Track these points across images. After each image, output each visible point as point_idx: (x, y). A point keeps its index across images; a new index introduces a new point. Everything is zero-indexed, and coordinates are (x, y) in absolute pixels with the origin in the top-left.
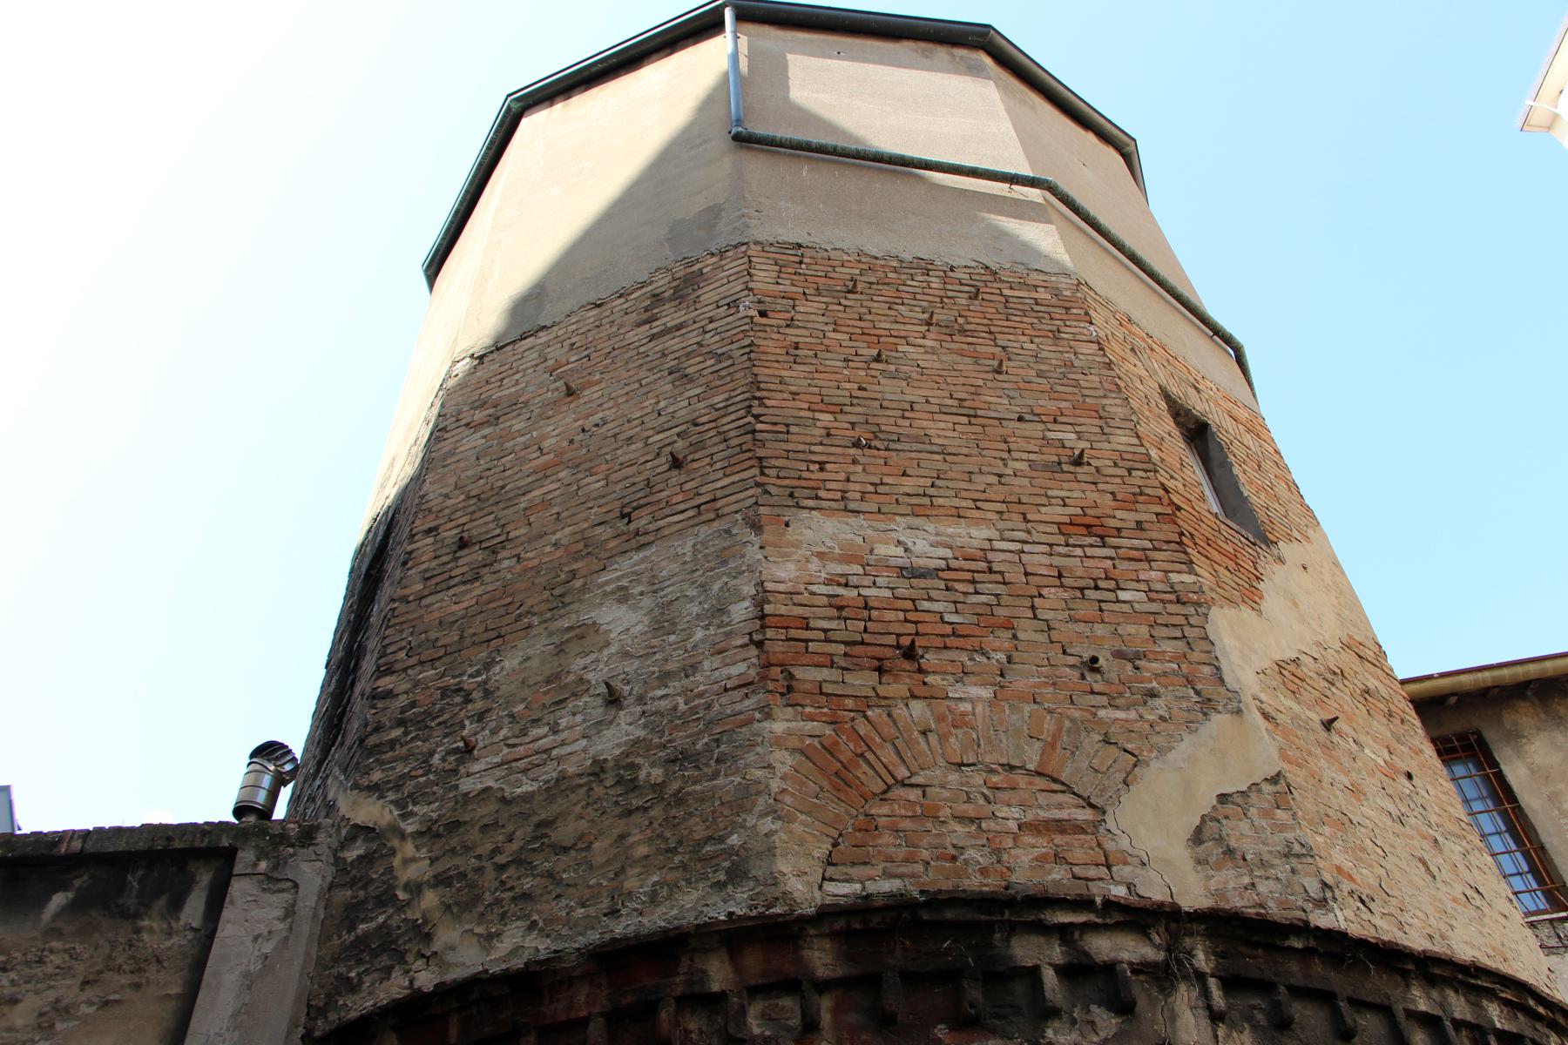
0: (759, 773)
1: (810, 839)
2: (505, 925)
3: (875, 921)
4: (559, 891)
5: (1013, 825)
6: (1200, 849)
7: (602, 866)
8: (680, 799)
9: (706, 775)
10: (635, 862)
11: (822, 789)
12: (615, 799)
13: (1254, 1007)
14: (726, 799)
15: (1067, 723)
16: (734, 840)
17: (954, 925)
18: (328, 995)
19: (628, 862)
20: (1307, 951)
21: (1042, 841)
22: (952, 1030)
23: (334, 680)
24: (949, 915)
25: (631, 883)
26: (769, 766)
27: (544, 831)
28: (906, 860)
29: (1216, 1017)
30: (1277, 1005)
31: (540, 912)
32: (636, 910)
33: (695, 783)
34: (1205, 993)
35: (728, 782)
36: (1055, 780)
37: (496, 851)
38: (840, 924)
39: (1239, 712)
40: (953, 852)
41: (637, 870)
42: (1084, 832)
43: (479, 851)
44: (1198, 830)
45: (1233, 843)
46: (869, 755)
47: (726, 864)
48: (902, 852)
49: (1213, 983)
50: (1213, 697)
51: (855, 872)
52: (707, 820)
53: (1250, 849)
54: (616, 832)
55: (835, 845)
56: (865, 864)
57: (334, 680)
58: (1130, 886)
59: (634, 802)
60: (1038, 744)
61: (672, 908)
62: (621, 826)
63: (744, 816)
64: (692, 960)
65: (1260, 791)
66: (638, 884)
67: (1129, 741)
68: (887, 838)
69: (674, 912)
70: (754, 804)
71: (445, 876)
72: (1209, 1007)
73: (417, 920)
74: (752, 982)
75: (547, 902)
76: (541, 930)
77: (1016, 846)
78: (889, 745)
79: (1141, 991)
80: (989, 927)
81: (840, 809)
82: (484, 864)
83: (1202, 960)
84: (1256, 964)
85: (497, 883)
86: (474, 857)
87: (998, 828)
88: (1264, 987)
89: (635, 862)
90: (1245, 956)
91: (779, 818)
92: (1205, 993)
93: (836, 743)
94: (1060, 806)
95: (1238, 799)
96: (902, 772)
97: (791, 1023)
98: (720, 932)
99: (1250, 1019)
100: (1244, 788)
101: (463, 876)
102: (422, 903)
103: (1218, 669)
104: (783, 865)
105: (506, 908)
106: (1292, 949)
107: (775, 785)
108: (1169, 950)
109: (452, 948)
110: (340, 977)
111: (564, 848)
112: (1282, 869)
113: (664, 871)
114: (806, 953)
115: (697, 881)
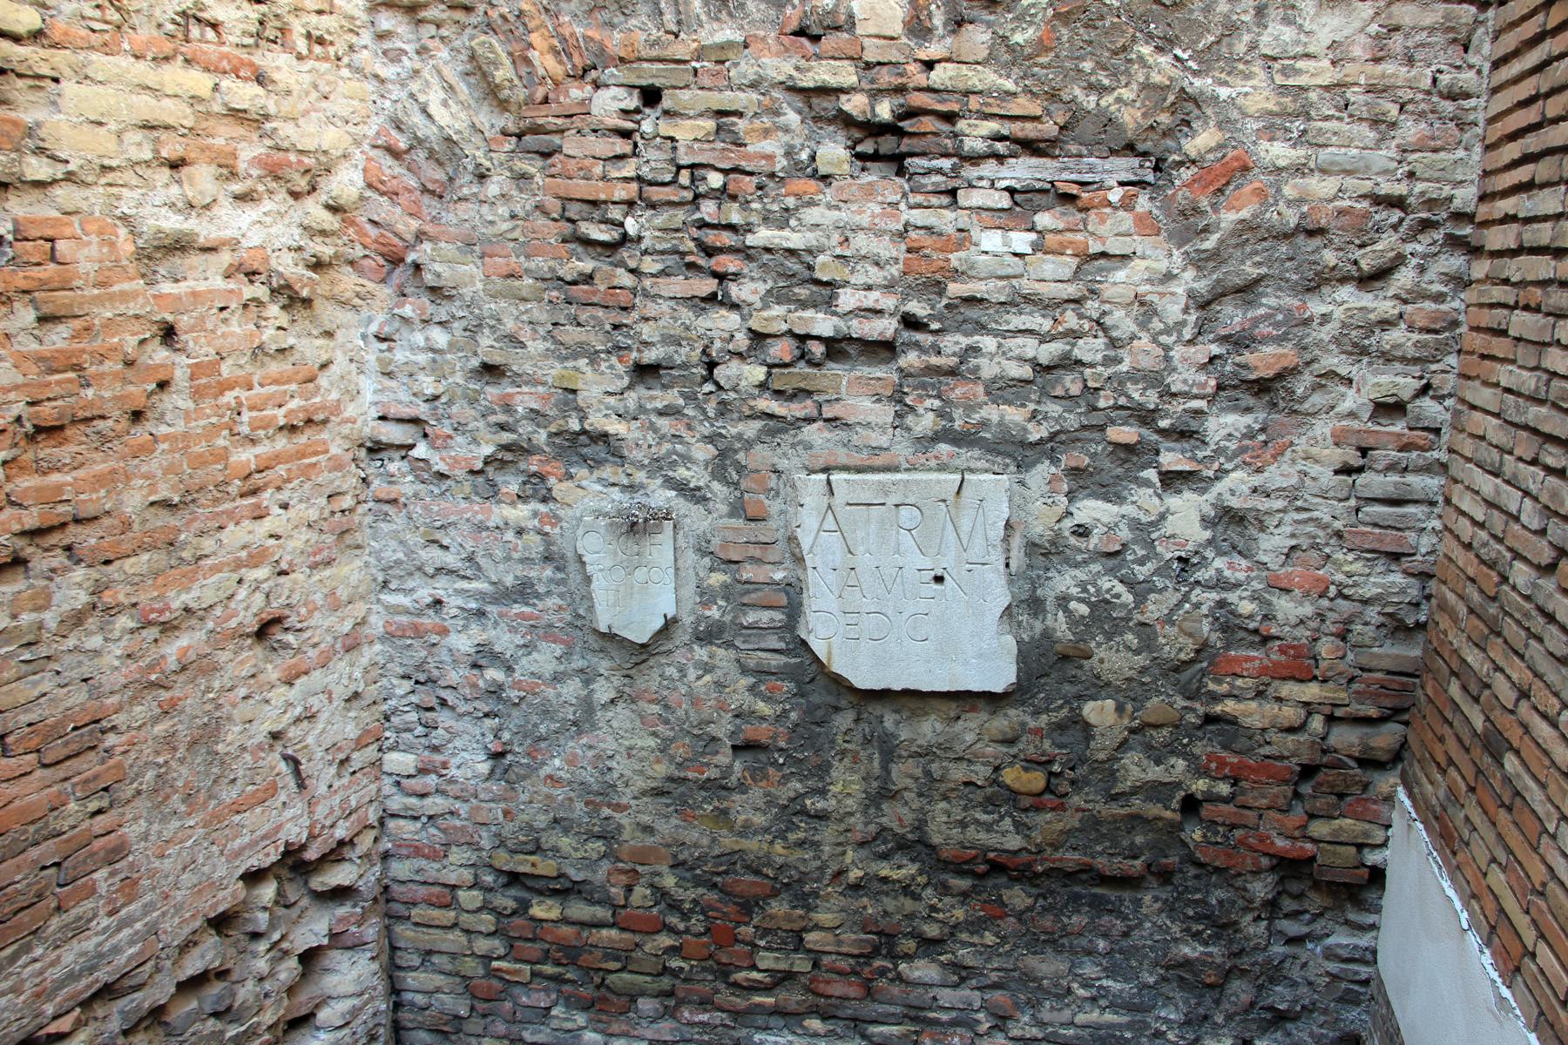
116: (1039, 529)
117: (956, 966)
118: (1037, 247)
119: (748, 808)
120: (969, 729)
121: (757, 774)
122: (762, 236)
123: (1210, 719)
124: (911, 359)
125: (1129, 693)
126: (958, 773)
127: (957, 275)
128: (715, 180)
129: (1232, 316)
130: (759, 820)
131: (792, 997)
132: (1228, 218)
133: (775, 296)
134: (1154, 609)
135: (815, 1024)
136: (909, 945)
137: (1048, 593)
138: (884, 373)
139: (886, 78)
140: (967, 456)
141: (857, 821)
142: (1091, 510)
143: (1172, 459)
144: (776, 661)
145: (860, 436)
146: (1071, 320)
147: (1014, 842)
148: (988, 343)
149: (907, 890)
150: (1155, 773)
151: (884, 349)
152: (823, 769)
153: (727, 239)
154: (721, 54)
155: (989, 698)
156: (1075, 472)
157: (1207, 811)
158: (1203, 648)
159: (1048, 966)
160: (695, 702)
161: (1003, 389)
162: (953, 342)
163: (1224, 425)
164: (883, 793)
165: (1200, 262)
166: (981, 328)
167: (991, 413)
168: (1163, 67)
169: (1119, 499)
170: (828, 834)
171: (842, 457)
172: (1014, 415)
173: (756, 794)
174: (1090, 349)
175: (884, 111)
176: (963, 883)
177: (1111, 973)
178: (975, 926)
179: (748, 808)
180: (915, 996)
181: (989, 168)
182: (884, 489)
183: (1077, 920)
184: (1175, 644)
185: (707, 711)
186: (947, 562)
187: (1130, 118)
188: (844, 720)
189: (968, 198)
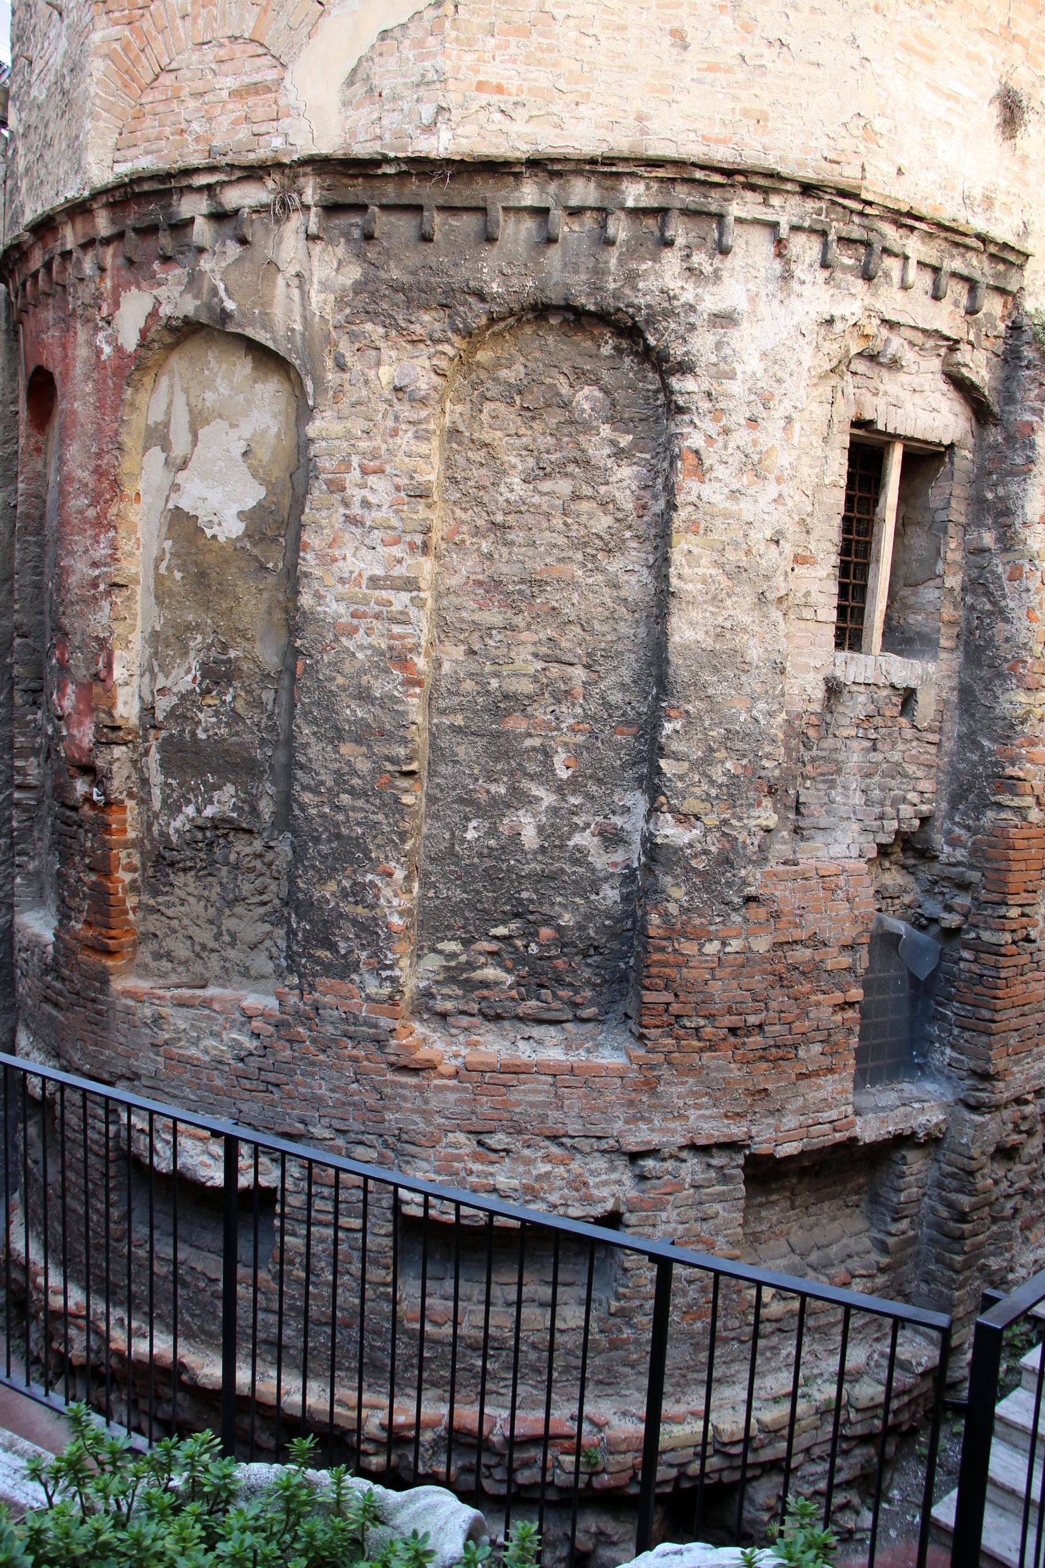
6: (349, 92)
13: (352, 225)
20: (400, 174)
23: (888, 1481)
24: (146, 187)
28: (157, 139)
44: (354, 71)
57: (888, 1481)
73: (204, 1485)
80: (168, 193)
84: (356, 190)
87: (215, 99)
90: (347, 186)
100: (404, 20)
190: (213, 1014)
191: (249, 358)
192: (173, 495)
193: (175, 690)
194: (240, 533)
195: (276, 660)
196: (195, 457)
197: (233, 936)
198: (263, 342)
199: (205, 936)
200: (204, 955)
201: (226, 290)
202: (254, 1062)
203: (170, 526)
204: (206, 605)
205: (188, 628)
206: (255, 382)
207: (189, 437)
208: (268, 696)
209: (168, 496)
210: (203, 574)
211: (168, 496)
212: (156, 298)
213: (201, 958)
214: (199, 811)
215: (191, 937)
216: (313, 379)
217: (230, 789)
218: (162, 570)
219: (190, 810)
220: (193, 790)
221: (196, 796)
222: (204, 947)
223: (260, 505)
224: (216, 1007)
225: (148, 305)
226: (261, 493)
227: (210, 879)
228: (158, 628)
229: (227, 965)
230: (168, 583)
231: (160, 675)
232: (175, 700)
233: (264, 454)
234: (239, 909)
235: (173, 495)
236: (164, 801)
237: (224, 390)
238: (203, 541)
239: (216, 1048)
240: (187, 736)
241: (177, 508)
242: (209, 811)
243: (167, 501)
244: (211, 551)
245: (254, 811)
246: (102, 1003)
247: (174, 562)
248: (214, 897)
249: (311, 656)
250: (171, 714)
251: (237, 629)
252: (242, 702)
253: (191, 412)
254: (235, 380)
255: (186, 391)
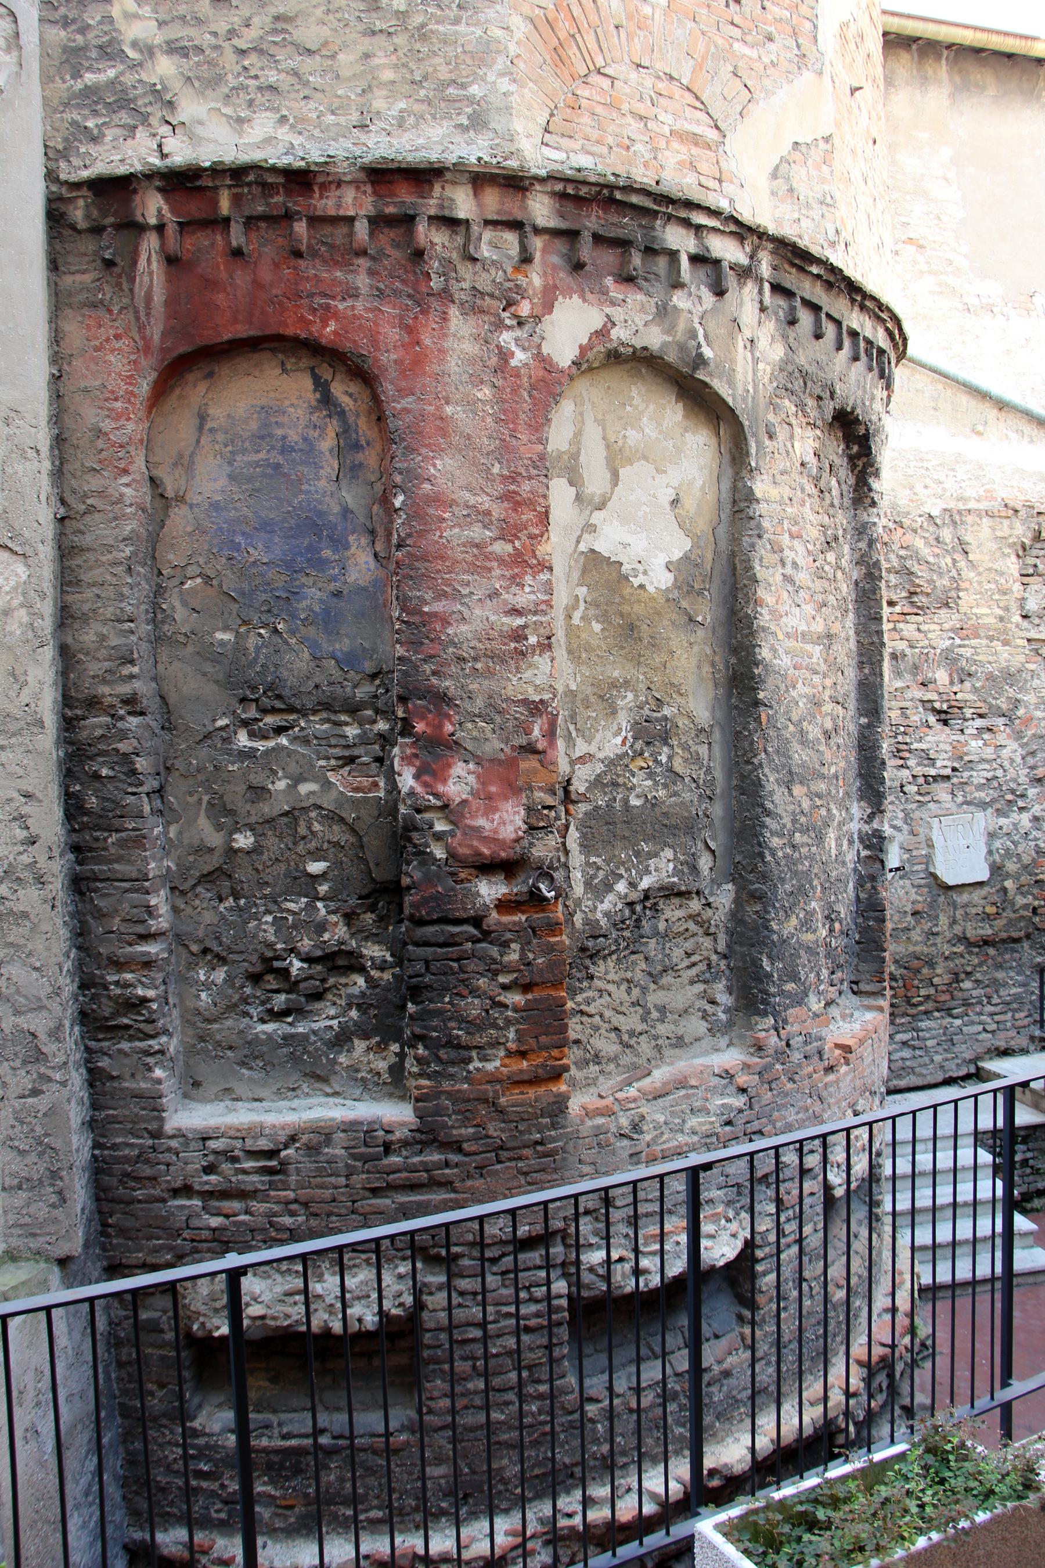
0: (499, 33)
1: (536, 106)
2: (255, 112)
3: (584, 191)
4: (307, 92)
5: (666, 130)
7: (349, 79)
8: (424, 35)
9: (448, 18)
10: (382, 85)
11: (545, 61)
12: (357, 14)
14: (468, 48)
15: (712, 48)
16: (475, 90)
17: (633, 207)
18: (66, 140)
19: (375, 82)
21: (683, 149)
22: (616, 282)
24: (635, 199)
25: (379, 103)
26: (507, 29)
27: (285, 26)
29: (763, 309)
30: (793, 309)
31: (289, 109)
32: (384, 130)
33: (438, 23)
34: (761, 292)
35: (468, 32)
36: (697, 98)
37: (232, 33)
38: (559, 187)
39: (820, 73)
40: (627, 142)
41: (385, 92)
42: (709, 148)
43: (213, 28)
44: (777, 168)
45: (795, 185)
46: (577, 36)
47: (469, 110)
48: (595, 134)
49: (767, 286)
50: (808, 54)
51: (565, 142)
52: (449, 64)
53: (802, 190)
54: (361, 49)
55: (552, 115)
56: (571, 137)
58: (732, 201)
59: (378, 23)
60: (691, 62)
61: (419, 136)
62: (366, 44)
63: (484, 70)
64: (443, 188)
65: (817, 146)
66: (386, 106)
67: (749, 78)
68: (586, 119)
69: (421, 141)
70: (494, 61)
71: (178, 45)
72: (761, 302)
74: (490, 217)
75: (295, 100)
76: (292, 126)
77: (667, 148)
78: (592, 32)
79: (731, 280)
81: (557, 84)
82: (221, 43)
83: (765, 269)
85: (239, 68)
86: (210, 33)
88: (788, 294)
89: (382, 85)
91: (514, 81)
92: (761, 292)
93: (556, 19)
94: (698, 122)
95: (804, 149)
96: (600, 62)
97: (510, 252)
98: (470, 172)
99: (776, 314)
101: (199, 50)
102: (157, 68)
103: (815, 27)
104: (518, 126)
105: (252, 96)
106: (810, 273)
107: (513, 49)
108: (751, 257)
109: (200, 123)
110: (74, 123)
111: (309, 50)
112: (816, 212)
113: (411, 100)
114: (530, 202)
115: (442, 118)
116: (991, 829)
117: (977, 981)
118: (985, 744)
119: (916, 935)
120: (977, 896)
121: (918, 922)
122: (915, 746)
123: (1036, 882)
124: (955, 780)
125: (1016, 877)
126: (974, 911)
127: (966, 754)
128: (902, 729)
129: (1031, 761)
130: (919, 939)
131: (930, 1006)
132: (1029, 733)
133: (918, 764)
134: (1020, 849)
135: (936, 1014)
136: (963, 976)
137: (993, 848)
138: (946, 785)
139: (945, 697)
140: (972, 808)
141: (947, 933)
142: (1002, 821)
143: (1021, 804)
144: (923, 882)
145: (943, 806)
146: (995, 766)
147: (990, 932)
148: (974, 774)
149: (962, 956)
150: (1025, 901)
151: (948, 778)
152: (937, 917)
153: (905, 747)
154: (901, 690)
155: (980, 884)
156: (997, 810)
157: (1039, 911)
158: (1033, 860)
159: (1000, 975)
160: (900, 900)
161: (980, 787)
162: (966, 774)
163: (1032, 792)
164: (954, 922)
165: (1022, 746)
166: (972, 769)
167: (977, 794)
168: (1011, 692)
169: (1008, 817)
170: (939, 940)
171: (940, 812)
172: (982, 794)
173: (918, 930)
174: (999, 773)
175: (945, 707)
176: (976, 950)
177: (1018, 974)
178: (980, 965)
179: (916, 935)
180: (966, 995)
181: (970, 722)
182: (954, 820)
183: (1007, 957)
184: (1026, 860)
185: (904, 902)
186: (971, 841)
187: (1004, 706)
188: (942, 899)
189: (967, 731)
190: (691, 1091)
191: (680, 405)
192: (585, 536)
193: (601, 755)
194: (669, 584)
195: (707, 714)
196: (614, 498)
197: (662, 1010)
198: (724, 396)
199: (631, 1022)
200: (632, 1042)
201: (706, 337)
202: (740, 1120)
203: (584, 571)
204: (637, 660)
205: (614, 685)
206: (686, 431)
207: (608, 475)
208: (703, 750)
209: (580, 537)
210: (632, 627)
211: (580, 537)
212: (607, 316)
213: (631, 1046)
214: (632, 885)
215: (616, 1029)
216: (757, 442)
217: (669, 853)
218: (576, 620)
219: (621, 887)
220: (623, 863)
221: (628, 870)
222: (632, 1033)
223: (686, 557)
224: (693, 1082)
225: (596, 321)
226: (687, 544)
227: (634, 957)
228: (574, 687)
229: (660, 1042)
230: (584, 635)
231: (579, 741)
232: (599, 768)
233: (689, 504)
234: (667, 979)
235: (585, 536)
236: (588, 884)
237: (650, 430)
238: (628, 590)
239: (700, 1124)
240: (618, 805)
241: (592, 551)
242: (645, 883)
243: (578, 542)
244: (639, 601)
245: (694, 869)
246: (554, 1140)
247: (592, 612)
248: (639, 976)
249: (771, 707)
250: (597, 783)
251: (672, 684)
252: (680, 760)
253: (608, 447)
254: (665, 425)
255: (601, 423)
